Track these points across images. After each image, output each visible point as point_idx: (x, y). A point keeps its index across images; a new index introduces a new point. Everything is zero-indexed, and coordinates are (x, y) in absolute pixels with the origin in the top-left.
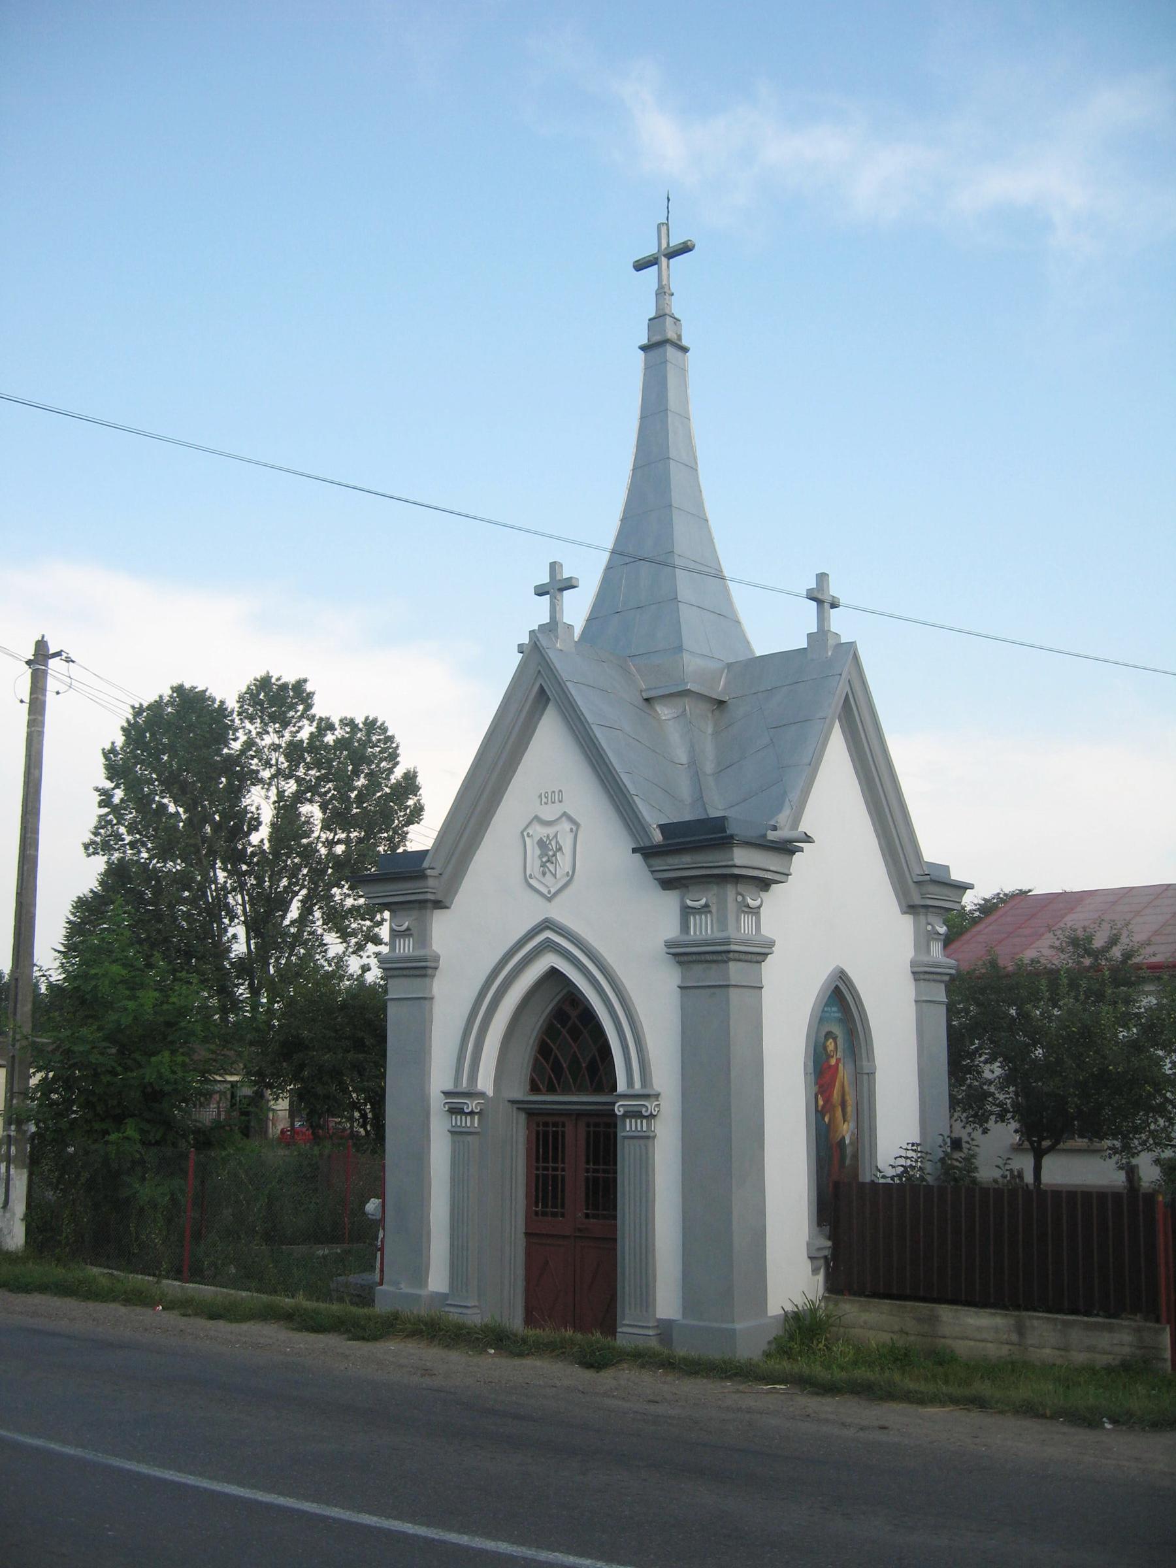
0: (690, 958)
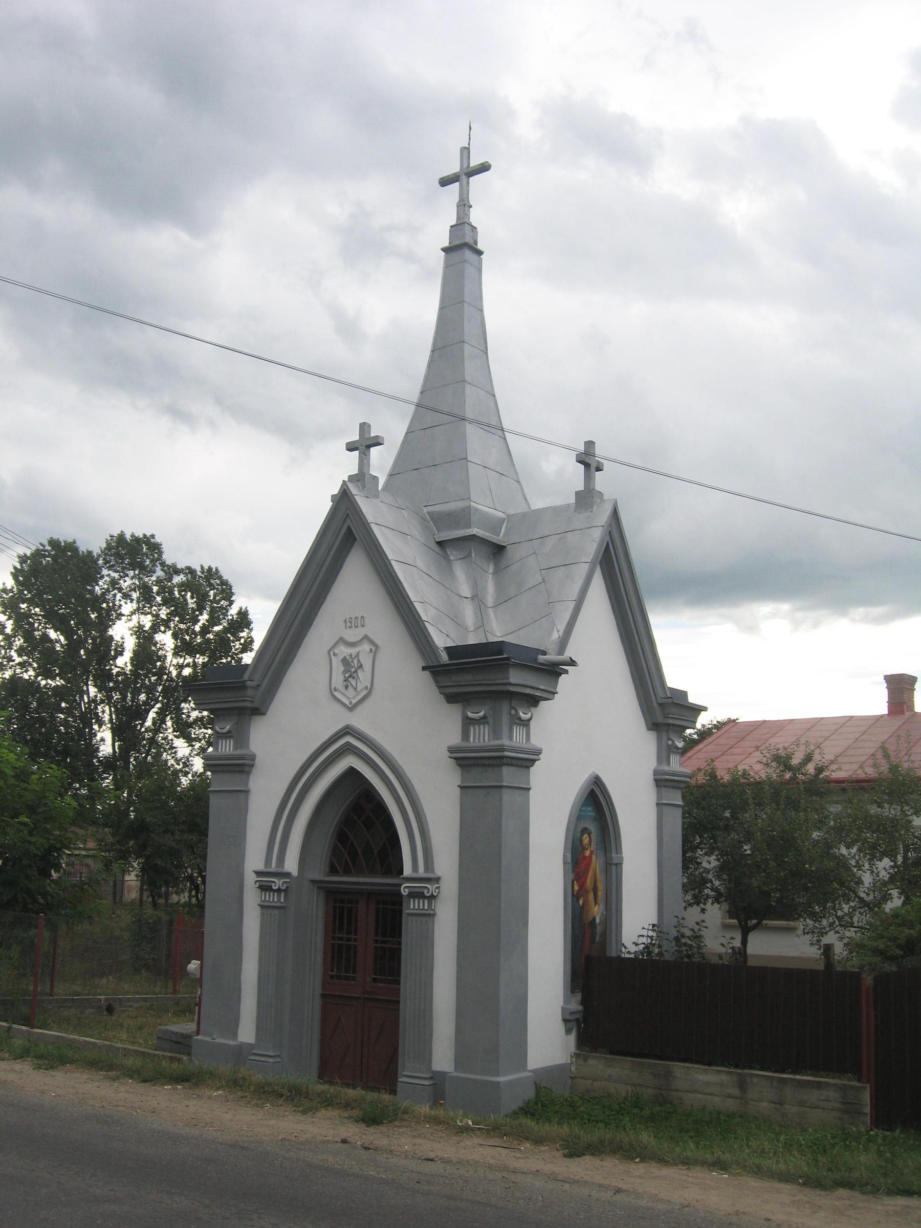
0: (468, 762)
